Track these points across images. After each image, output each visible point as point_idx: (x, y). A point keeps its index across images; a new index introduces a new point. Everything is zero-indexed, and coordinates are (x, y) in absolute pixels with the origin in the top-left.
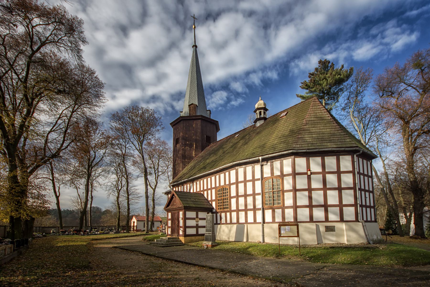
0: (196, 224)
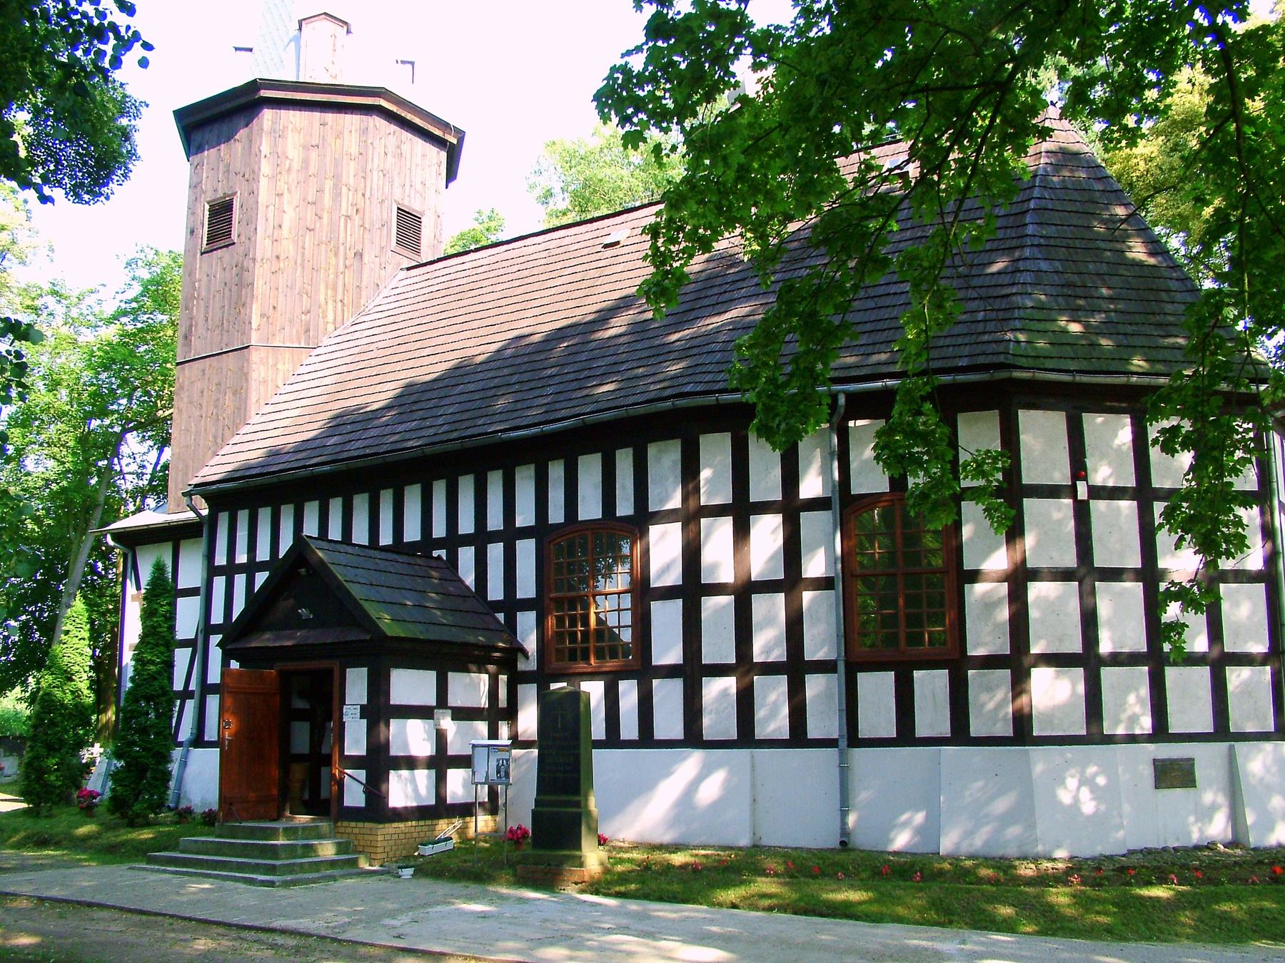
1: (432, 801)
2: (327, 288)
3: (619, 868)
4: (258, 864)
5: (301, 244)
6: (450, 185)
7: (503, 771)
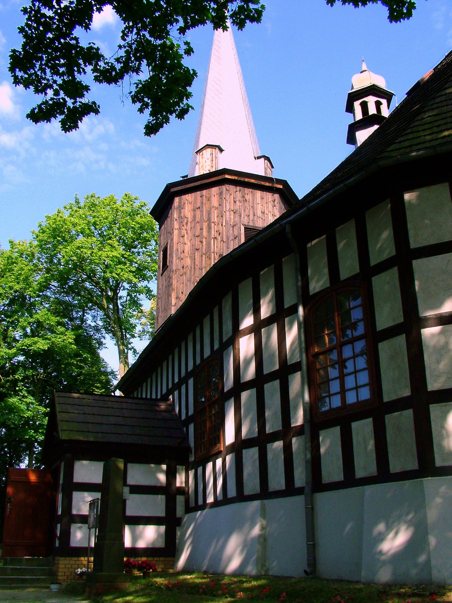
5: (193, 258)
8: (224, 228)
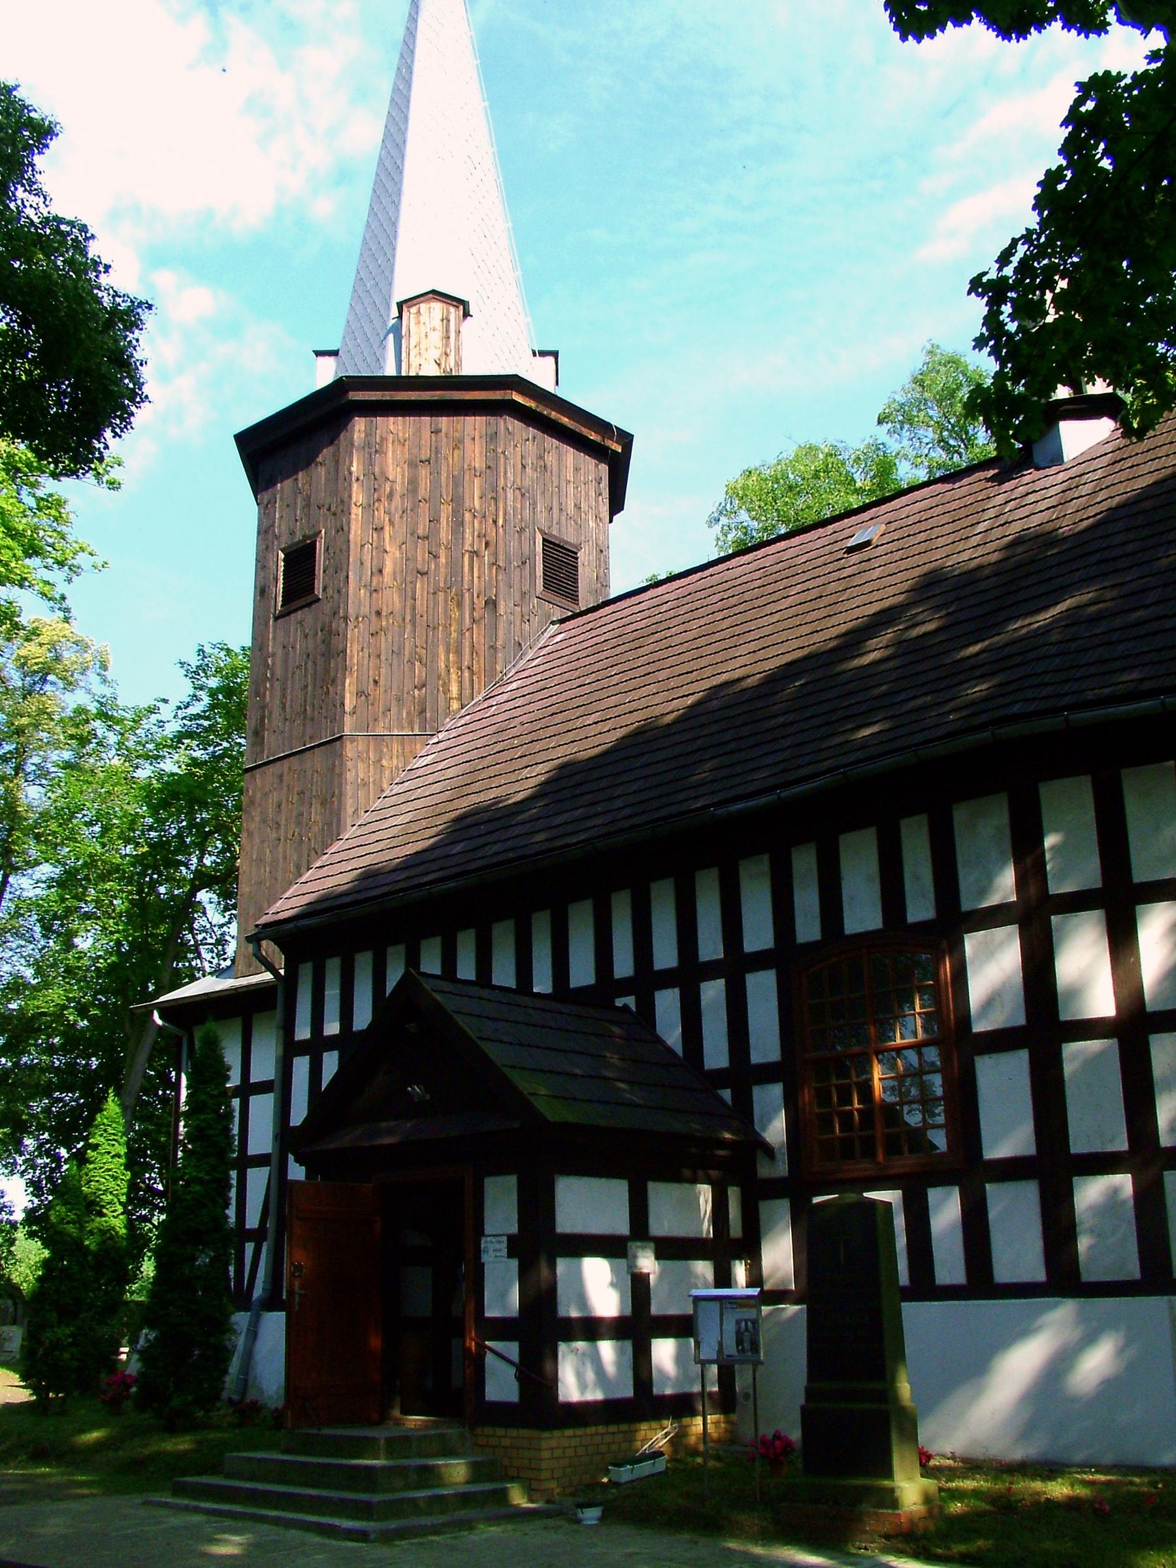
0: (510, 1255)
1: (627, 1391)
2: (448, 652)
3: (956, 1507)
4: (342, 1500)
6: (615, 517)
7: (748, 1338)
8: (501, 530)
